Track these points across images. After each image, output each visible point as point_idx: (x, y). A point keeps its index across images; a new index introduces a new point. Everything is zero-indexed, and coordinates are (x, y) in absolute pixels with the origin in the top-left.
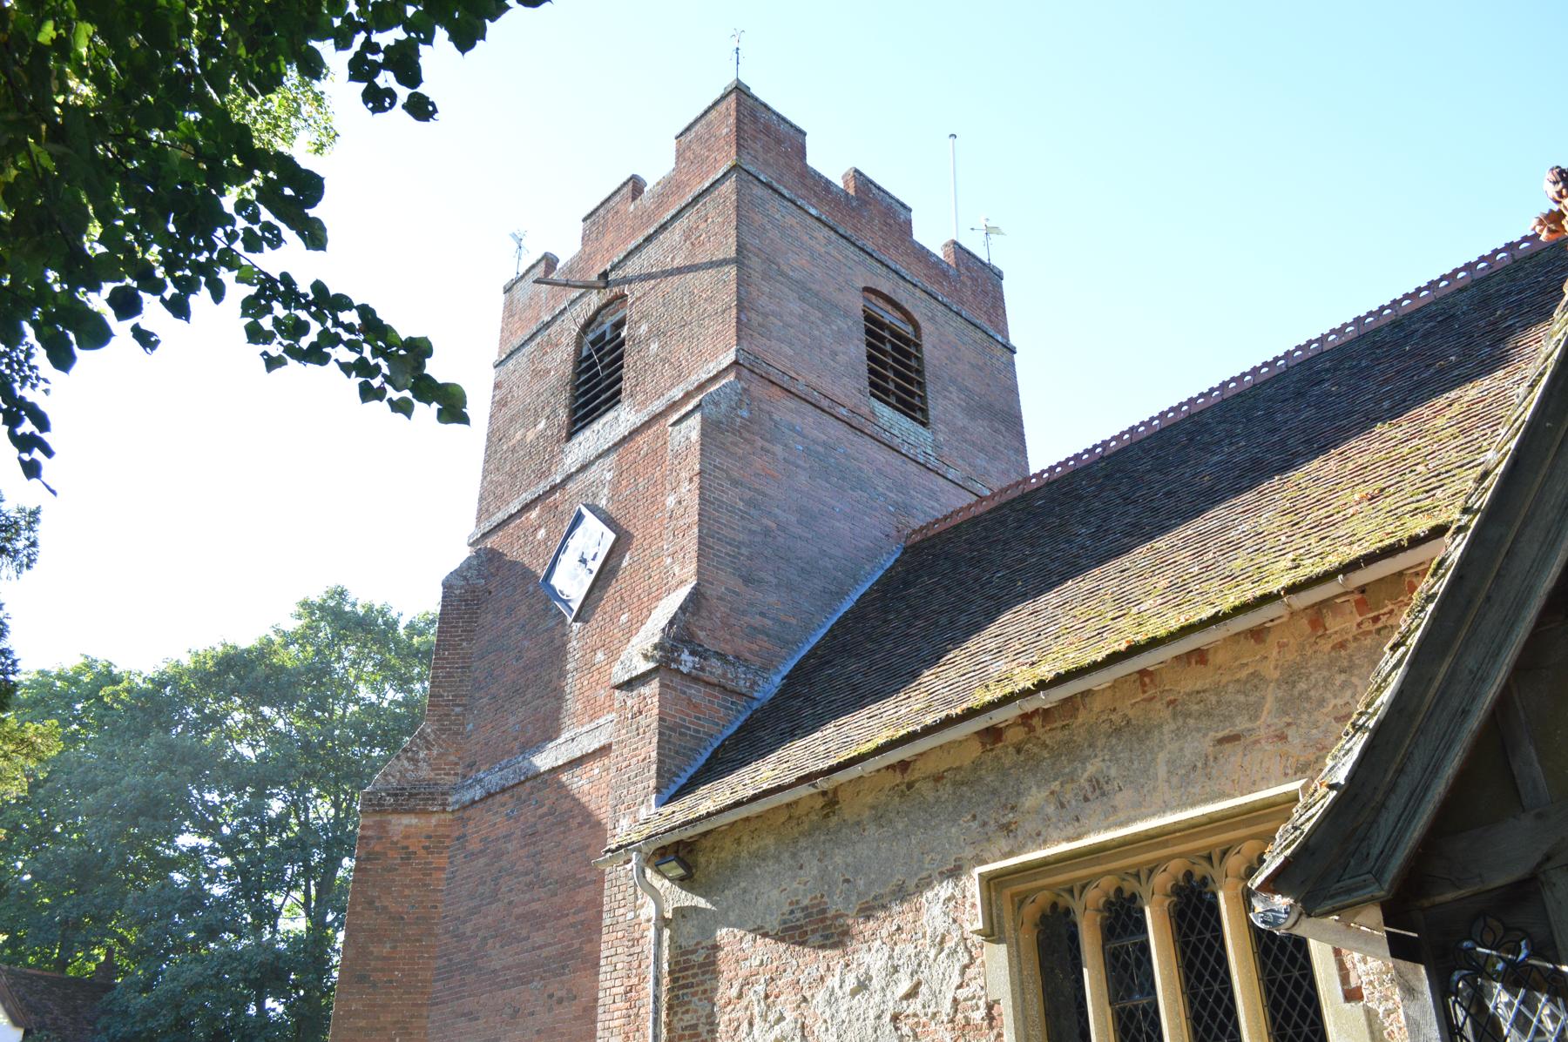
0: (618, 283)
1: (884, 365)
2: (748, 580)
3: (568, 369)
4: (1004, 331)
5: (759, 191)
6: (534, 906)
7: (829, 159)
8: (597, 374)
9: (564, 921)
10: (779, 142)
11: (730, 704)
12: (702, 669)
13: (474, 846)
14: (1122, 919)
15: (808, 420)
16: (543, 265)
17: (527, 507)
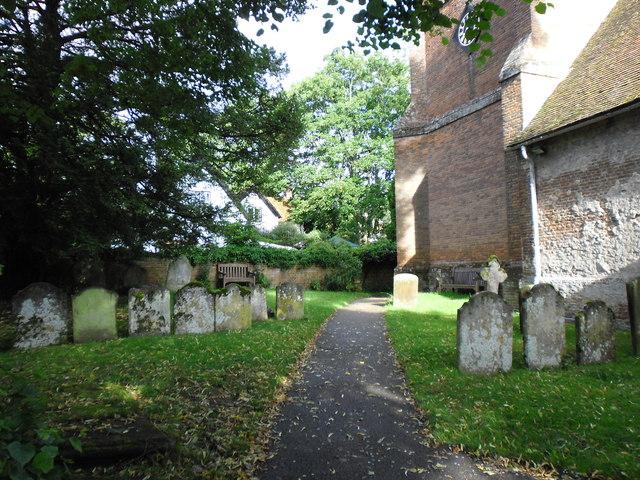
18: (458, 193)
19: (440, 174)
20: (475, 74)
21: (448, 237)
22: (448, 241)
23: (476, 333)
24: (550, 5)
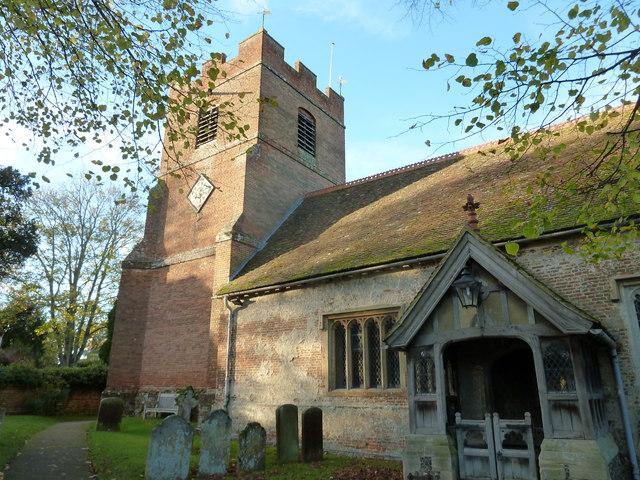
0: (215, 94)
1: (303, 129)
2: (258, 211)
4: (342, 121)
5: (269, 73)
7: (291, 59)
8: (206, 135)
10: (275, 52)
11: (249, 250)
14: (355, 328)
15: (278, 156)
23: (163, 448)
24: (516, 38)
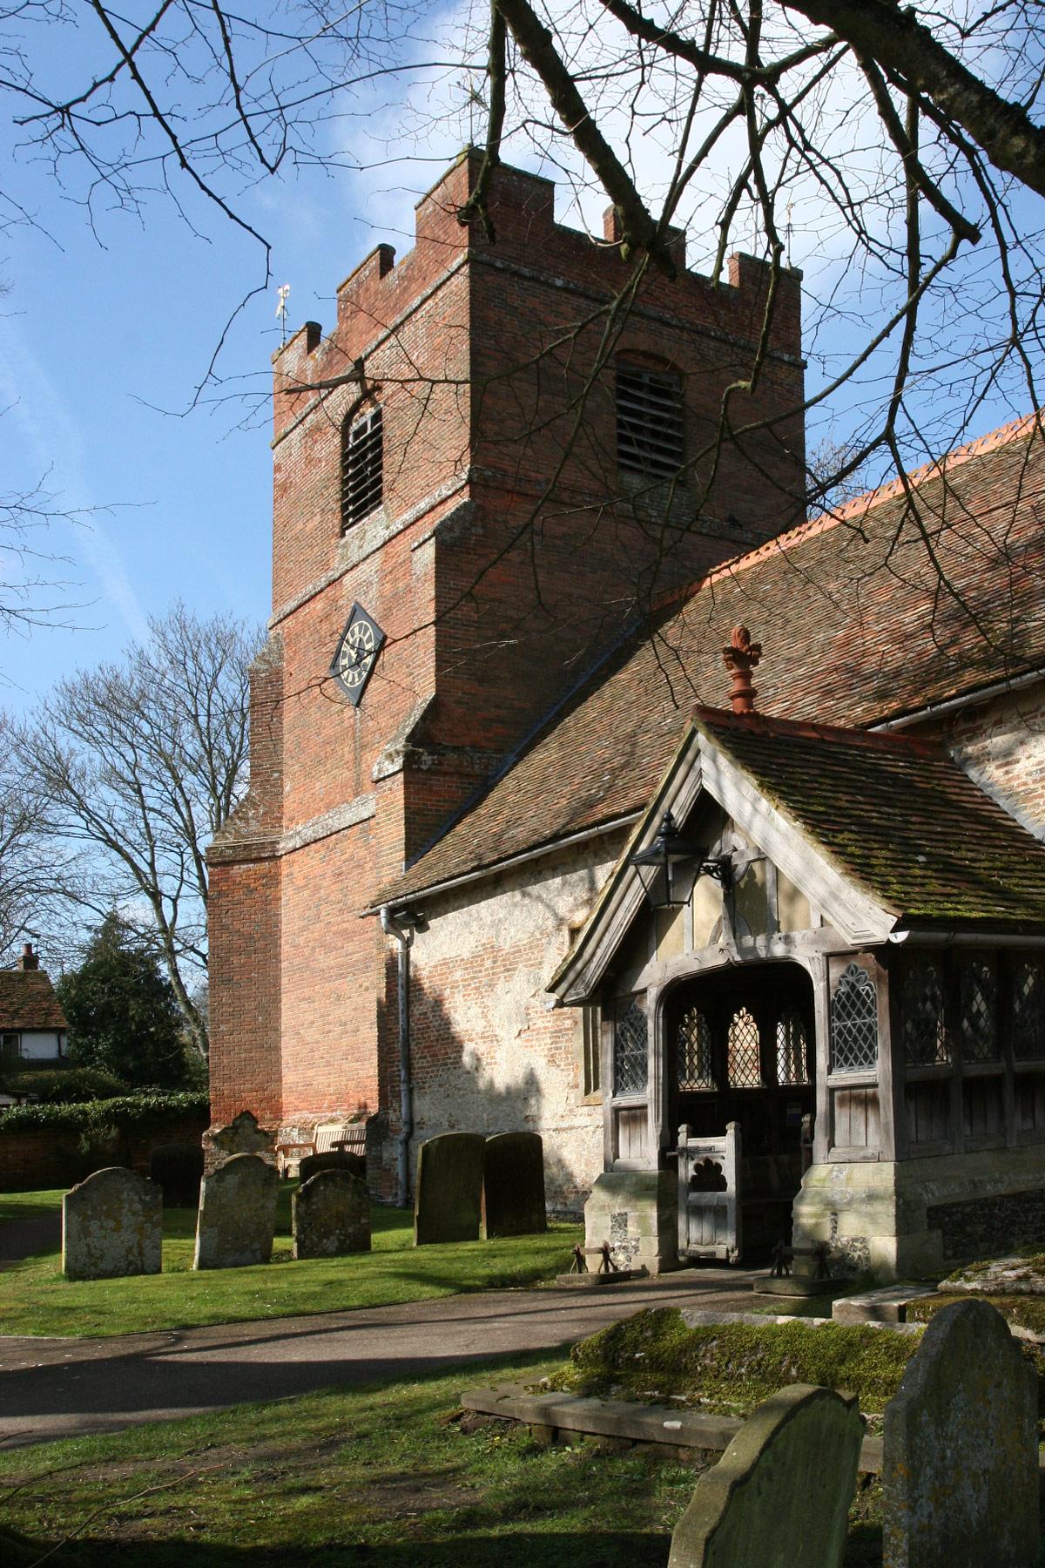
3: (337, 460)
6: (345, 925)
9: (366, 936)
12: (440, 764)
13: (301, 882)
16: (304, 335)
17: (424, 302)
18: (329, 979)
19: (301, 940)
20: (363, 747)
21: (311, 1065)
22: (311, 1073)
